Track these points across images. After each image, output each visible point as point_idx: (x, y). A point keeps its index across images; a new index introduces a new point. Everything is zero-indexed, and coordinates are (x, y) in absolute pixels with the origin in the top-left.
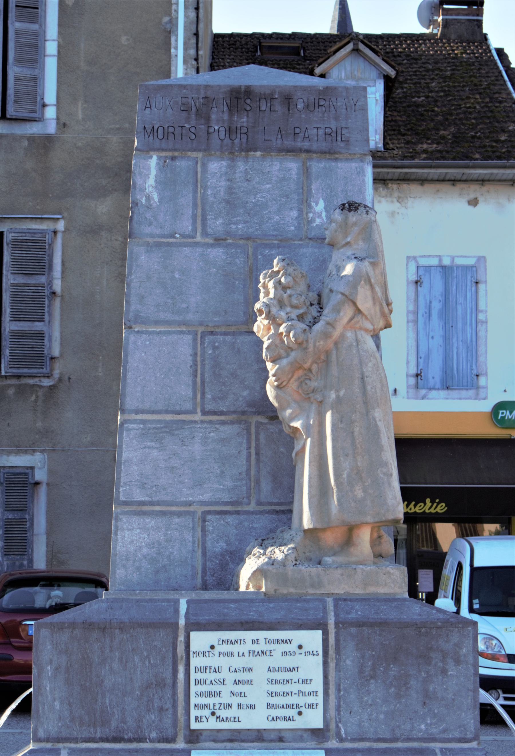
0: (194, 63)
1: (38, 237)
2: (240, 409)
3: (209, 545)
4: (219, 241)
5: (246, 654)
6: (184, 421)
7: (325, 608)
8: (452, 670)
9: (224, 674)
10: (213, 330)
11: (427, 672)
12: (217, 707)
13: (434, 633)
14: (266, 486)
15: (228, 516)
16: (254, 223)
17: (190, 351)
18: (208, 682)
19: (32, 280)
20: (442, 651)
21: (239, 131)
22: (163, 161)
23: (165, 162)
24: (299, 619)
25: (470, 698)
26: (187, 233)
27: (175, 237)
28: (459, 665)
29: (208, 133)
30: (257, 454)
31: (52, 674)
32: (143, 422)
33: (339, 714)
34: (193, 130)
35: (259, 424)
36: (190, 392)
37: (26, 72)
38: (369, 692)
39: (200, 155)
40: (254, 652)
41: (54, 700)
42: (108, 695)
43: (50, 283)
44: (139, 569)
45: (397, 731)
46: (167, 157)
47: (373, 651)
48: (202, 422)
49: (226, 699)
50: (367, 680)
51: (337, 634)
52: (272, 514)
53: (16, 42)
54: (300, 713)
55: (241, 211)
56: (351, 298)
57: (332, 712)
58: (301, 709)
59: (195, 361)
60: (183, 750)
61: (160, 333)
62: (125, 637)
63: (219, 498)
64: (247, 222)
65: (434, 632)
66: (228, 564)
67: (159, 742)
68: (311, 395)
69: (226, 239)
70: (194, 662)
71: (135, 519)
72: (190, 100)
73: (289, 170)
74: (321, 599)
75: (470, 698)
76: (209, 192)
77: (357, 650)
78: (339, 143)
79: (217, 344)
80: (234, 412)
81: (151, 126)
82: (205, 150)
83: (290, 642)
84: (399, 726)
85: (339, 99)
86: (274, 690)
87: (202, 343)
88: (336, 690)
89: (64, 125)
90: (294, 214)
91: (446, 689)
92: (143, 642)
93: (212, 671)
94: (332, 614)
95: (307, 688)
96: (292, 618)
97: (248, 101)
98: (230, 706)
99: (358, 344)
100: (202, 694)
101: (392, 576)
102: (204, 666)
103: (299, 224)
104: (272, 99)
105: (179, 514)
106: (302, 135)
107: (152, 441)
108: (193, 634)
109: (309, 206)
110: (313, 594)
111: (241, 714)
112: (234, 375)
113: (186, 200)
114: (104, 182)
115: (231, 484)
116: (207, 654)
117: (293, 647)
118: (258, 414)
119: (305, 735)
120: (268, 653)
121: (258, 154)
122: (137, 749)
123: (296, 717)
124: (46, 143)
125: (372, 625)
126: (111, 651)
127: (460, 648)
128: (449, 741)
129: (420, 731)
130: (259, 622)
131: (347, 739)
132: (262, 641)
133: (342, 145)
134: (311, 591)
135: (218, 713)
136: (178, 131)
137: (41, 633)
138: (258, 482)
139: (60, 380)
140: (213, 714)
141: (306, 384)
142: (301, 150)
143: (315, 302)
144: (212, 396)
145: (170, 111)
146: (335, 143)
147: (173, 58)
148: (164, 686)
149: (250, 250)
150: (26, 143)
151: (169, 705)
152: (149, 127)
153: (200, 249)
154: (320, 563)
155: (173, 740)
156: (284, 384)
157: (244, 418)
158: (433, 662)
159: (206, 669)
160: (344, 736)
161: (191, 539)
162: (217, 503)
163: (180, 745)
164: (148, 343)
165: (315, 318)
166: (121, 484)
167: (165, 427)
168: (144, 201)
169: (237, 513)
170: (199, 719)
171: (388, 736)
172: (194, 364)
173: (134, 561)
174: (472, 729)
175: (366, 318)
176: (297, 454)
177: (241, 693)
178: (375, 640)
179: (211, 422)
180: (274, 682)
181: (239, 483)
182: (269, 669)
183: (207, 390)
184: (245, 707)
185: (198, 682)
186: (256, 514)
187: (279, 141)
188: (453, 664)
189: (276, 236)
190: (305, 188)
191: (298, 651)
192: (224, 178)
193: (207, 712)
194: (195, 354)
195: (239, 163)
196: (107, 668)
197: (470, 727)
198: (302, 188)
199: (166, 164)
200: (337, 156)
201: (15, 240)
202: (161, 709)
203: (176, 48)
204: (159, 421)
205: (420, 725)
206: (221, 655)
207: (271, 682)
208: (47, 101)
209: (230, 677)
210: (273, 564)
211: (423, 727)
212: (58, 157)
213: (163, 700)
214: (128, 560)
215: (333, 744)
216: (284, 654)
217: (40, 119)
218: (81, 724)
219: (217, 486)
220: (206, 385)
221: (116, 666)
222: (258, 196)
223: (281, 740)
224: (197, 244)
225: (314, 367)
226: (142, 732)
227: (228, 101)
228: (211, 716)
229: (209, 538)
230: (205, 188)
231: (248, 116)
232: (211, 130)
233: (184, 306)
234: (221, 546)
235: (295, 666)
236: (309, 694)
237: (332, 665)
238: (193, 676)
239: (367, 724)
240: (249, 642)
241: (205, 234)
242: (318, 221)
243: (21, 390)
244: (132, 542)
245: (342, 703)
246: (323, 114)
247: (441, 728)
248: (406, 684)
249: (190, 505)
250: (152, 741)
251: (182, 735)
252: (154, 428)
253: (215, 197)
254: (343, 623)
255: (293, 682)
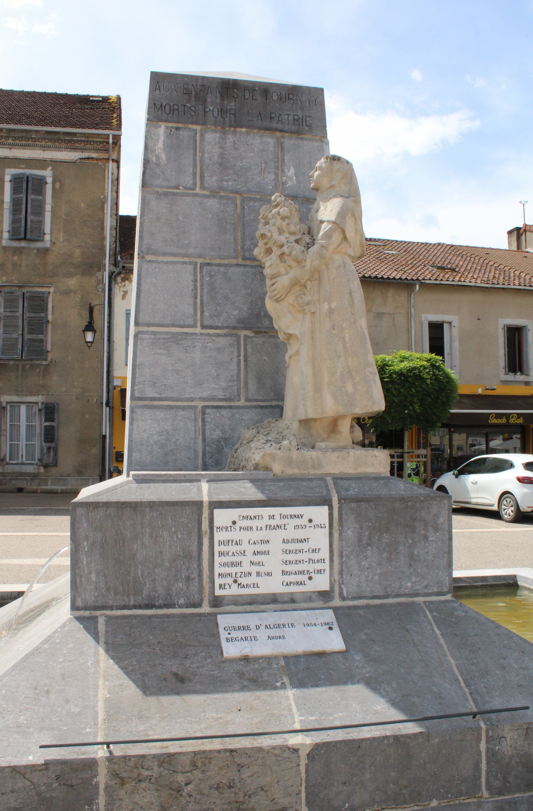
0: (115, 217)
1: (41, 295)
2: (231, 325)
3: (208, 433)
4: (214, 194)
5: (264, 528)
6: (187, 333)
7: (327, 486)
8: (432, 537)
9: (245, 546)
10: (209, 262)
11: (413, 539)
12: (238, 575)
13: (418, 506)
14: (252, 386)
15: (223, 410)
16: (241, 181)
17: (191, 278)
18: (230, 554)
19: (38, 315)
20: (425, 521)
21: (228, 112)
22: (169, 131)
23: (171, 131)
24: (308, 496)
25: (446, 558)
26: (189, 186)
27: (179, 189)
28: (437, 532)
29: (205, 112)
30: (246, 361)
31: (88, 549)
32: (154, 333)
33: (342, 577)
34: (193, 108)
35: (246, 337)
36: (191, 311)
37: (36, 218)
38: (366, 558)
39: (198, 128)
40: (270, 526)
41: (90, 572)
42: (140, 567)
43: (46, 317)
44: (151, 452)
45: (388, 589)
46: (173, 127)
47: (369, 522)
48: (202, 334)
49: (246, 568)
50: (364, 547)
51: (340, 508)
52: (258, 408)
53: (32, 204)
54: (310, 578)
55: (231, 172)
56: (341, 226)
57: (336, 577)
58: (311, 575)
59: (195, 288)
60: (209, 614)
61: (167, 262)
62: (155, 515)
63: (216, 396)
64: (236, 180)
65: (418, 505)
66: (223, 448)
67: (187, 607)
68: (305, 307)
69: (219, 192)
70: (218, 536)
71: (147, 411)
72: (191, 87)
73: (268, 144)
74: (322, 479)
75: (446, 558)
76: (206, 156)
77: (356, 522)
78: (304, 127)
79: (213, 273)
80: (227, 327)
81: (160, 103)
82: (203, 124)
83: (302, 517)
84: (390, 585)
85: (303, 95)
86: (288, 559)
87: (201, 272)
88: (339, 556)
89: (54, 243)
90: (272, 176)
91: (427, 552)
92: (171, 519)
93: (234, 544)
94: (334, 491)
95: (316, 556)
96: (302, 496)
97: (235, 91)
98: (250, 574)
99: (345, 266)
100: (225, 565)
101: (378, 459)
102: (227, 539)
103: (276, 184)
104: (254, 90)
105: (184, 408)
106: (276, 119)
107: (161, 349)
108: (216, 512)
109: (283, 171)
110: (314, 474)
111: (259, 580)
112: (226, 298)
113: (187, 161)
114: (72, 270)
115: (225, 384)
116: (229, 529)
117: (304, 521)
118: (246, 330)
119: (314, 597)
120: (283, 527)
121: (244, 130)
122: (167, 615)
123: (307, 582)
124: (46, 251)
125: (368, 500)
126: (142, 527)
127: (439, 518)
128: (429, 595)
129: (407, 588)
130: (274, 500)
131: (348, 597)
132: (277, 517)
133: (307, 128)
134: (312, 472)
135: (240, 580)
136: (181, 108)
137: (78, 512)
138: (246, 383)
139: (51, 362)
140: (235, 581)
141: (302, 298)
142: (276, 130)
143: (306, 232)
144: (210, 314)
145: (174, 93)
146: (301, 127)
147: (106, 214)
148: (191, 558)
149: (238, 202)
150: (35, 251)
151: (195, 575)
152: (158, 104)
153: (198, 199)
154: (313, 448)
155: (199, 605)
156: (283, 297)
157: (234, 332)
158: (417, 530)
159: (228, 542)
160: (346, 595)
161: (193, 429)
162: (213, 399)
163: (206, 609)
164: (157, 270)
165: (308, 244)
166: (136, 383)
167: (171, 338)
168: (154, 160)
169: (230, 407)
170: (223, 586)
171: (381, 593)
172: (194, 288)
173: (147, 446)
174: (447, 584)
175: (350, 246)
176: (290, 357)
177: (259, 563)
178: (371, 513)
179: (208, 335)
180: (288, 552)
181: (231, 384)
182: (284, 541)
183: (205, 309)
184: (263, 574)
185: (221, 554)
186: (245, 409)
187: (260, 122)
188: (433, 531)
189: (258, 192)
190: (279, 158)
191: (308, 524)
192: (217, 146)
193: (230, 580)
194: (196, 281)
195: (229, 136)
196: (139, 542)
197: (446, 583)
198: (278, 158)
199: (172, 133)
200: (303, 136)
201: (30, 296)
202: (188, 578)
203: (107, 210)
204: (167, 333)
205: (407, 583)
206: (242, 530)
207: (286, 552)
208: (46, 232)
209: (250, 549)
210: (280, 449)
211: (409, 584)
212: (51, 259)
213: (189, 570)
214: (142, 445)
215: (337, 602)
216: (297, 527)
217: (43, 240)
218: (116, 594)
219: (214, 386)
220: (204, 305)
221: (146, 540)
222: (244, 161)
223: (293, 601)
224: (196, 195)
225: (309, 284)
226: (171, 599)
227: (220, 90)
228: (233, 584)
229: (208, 427)
230: (203, 152)
231: (235, 101)
232: (207, 110)
233: (187, 242)
234: (217, 434)
235: (306, 537)
236: (318, 561)
237: (336, 535)
238: (217, 549)
239: (364, 585)
240: (266, 517)
241: (203, 187)
242: (290, 184)
243: (33, 367)
244: (145, 430)
245: (344, 568)
246: (292, 105)
247: (423, 585)
248: (396, 549)
249: (192, 401)
250: (180, 607)
251: (207, 600)
252: (163, 338)
253: (211, 160)
254: (345, 500)
255: (304, 551)
